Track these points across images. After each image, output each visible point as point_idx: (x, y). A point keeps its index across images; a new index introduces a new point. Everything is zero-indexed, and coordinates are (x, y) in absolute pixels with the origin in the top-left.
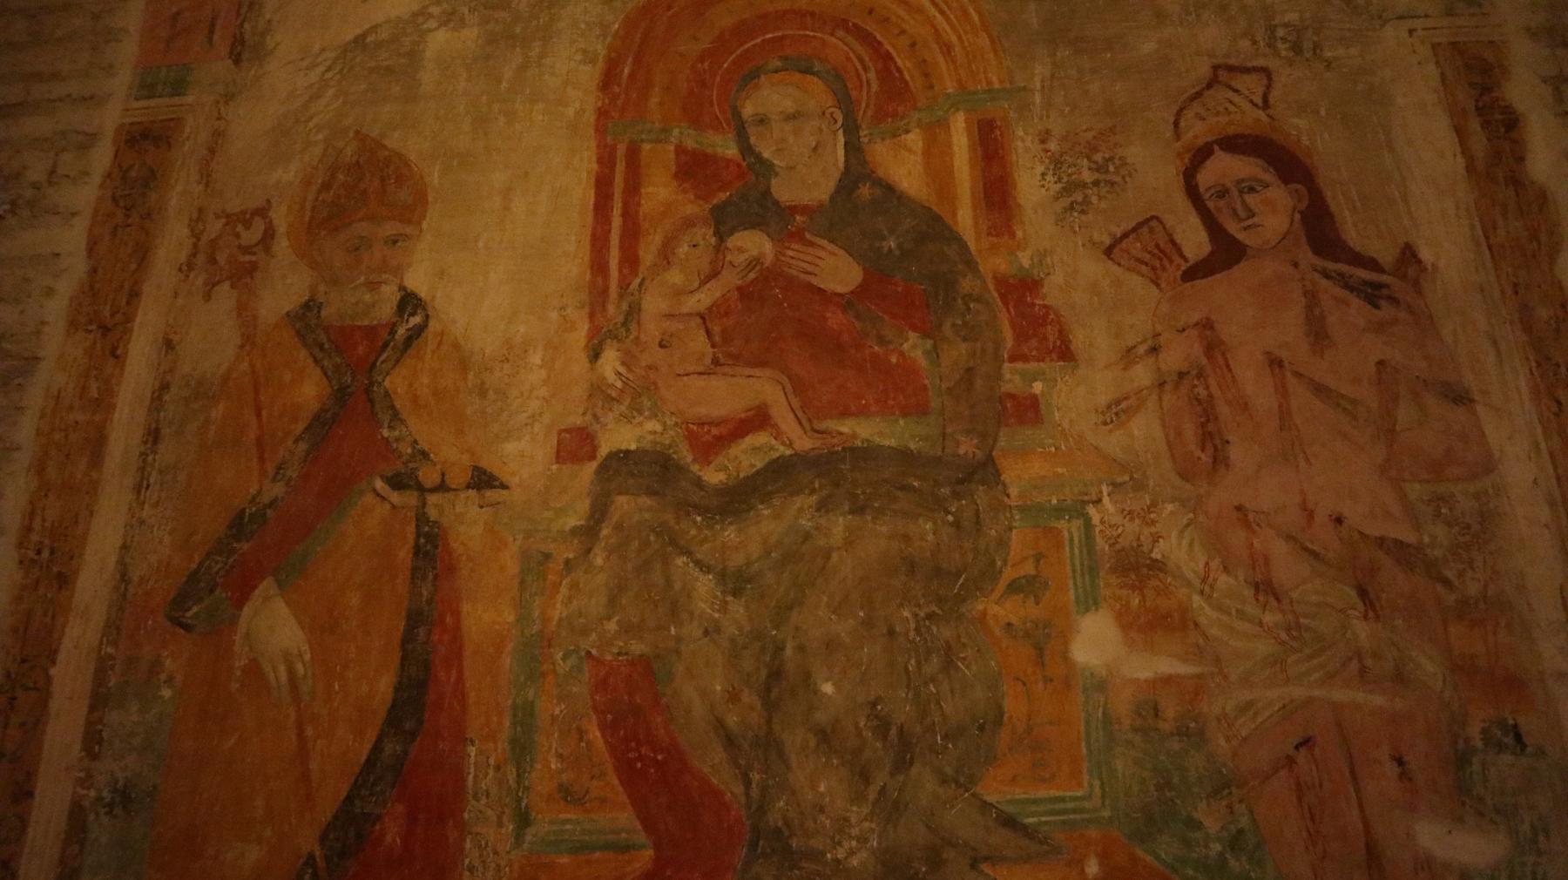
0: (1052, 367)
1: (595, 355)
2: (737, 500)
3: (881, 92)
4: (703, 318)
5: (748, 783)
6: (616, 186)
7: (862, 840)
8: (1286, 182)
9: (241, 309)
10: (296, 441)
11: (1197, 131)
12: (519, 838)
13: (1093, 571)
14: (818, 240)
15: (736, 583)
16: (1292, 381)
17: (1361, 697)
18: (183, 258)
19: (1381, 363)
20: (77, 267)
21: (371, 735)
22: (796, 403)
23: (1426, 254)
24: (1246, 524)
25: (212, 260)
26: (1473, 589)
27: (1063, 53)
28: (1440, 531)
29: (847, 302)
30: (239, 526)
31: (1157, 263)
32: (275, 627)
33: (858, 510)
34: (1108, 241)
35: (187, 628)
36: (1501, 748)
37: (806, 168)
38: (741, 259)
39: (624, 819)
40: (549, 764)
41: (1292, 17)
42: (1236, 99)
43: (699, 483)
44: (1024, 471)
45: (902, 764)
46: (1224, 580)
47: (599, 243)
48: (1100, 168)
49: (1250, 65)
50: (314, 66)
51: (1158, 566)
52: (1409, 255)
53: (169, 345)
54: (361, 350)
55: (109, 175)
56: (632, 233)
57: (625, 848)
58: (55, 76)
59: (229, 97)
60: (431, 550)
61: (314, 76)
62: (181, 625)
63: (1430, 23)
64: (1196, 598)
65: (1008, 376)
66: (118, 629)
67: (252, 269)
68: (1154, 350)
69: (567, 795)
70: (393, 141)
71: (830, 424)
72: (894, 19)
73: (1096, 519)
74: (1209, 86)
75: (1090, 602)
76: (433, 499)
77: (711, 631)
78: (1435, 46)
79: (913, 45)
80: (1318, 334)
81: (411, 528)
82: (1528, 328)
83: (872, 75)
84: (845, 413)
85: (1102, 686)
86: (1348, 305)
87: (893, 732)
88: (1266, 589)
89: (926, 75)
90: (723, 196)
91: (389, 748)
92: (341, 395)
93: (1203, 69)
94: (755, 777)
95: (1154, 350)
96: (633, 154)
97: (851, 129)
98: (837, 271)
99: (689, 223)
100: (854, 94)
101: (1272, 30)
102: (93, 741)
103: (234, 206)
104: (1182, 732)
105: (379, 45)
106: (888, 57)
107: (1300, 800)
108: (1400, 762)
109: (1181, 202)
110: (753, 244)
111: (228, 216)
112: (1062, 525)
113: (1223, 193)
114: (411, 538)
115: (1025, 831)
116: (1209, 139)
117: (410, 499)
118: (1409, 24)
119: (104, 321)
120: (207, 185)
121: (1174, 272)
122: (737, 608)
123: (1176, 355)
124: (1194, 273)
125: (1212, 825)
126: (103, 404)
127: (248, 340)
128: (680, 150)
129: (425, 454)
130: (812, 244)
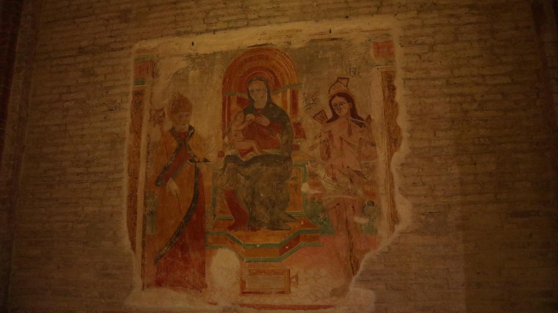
0: (302, 140)
1: (224, 138)
2: (248, 164)
3: (275, 85)
9: (161, 129)
11: (333, 92)
12: (214, 218)
15: (247, 178)
16: (344, 142)
17: (348, 197)
18: (149, 118)
19: (360, 139)
20: (130, 120)
21: (190, 203)
23: (372, 117)
24: (332, 168)
25: (154, 119)
26: (370, 179)
27: (309, 75)
28: (366, 169)
29: (267, 128)
30: (165, 169)
32: (173, 186)
33: (267, 165)
34: (314, 115)
36: (370, 205)
37: (261, 103)
38: (249, 119)
39: (230, 216)
40: (218, 208)
41: (354, 66)
43: (241, 161)
44: (296, 159)
45: (273, 207)
46: (328, 178)
47: (223, 116)
48: (314, 100)
50: (168, 78)
51: (316, 175)
52: (369, 117)
53: (149, 136)
54: (183, 137)
56: (229, 114)
58: (119, 80)
59: (153, 85)
60: (198, 172)
61: (169, 80)
63: (382, 67)
67: (161, 121)
68: (320, 136)
69: (221, 212)
70: (185, 95)
71: (264, 150)
75: (304, 181)
76: (197, 164)
77: (243, 186)
78: (382, 72)
80: (350, 133)
82: (389, 132)
84: (266, 148)
85: (306, 195)
90: (245, 107)
91: (193, 205)
92: (180, 145)
93: (336, 79)
95: (320, 136)
96: (229, 98)
97: (269, 93)
98: (265, 121)
99: (239, 112)
101: (350, 69)
102: (145, 204)
103: (157, 108)
104: (318, 202)
105: (180, 74)
106: (276, 77)
108: (353, 207)
110: (250, 116)
112: (301, 168)
115: (293, 218)
117: (194, 164)
118: (377, 67)
119: (136, 131)
122: (248, 182)
123: (323, 138)
125: (321, 217)
126: (138, 147)
127: (163, 135)
128: (238, 97)
129: (196, 156)
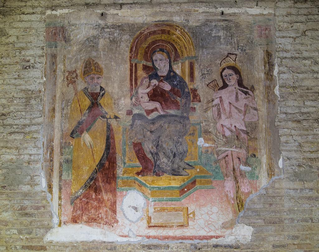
1: (131, 99)
2: (153, 122)
5: (154, 159)
6: (133, 69)
8: (236, 74)
10: (86, 110)
11: (224, 65)
13: (201, 133)
14: (164, 82)
22: (161, 107)
31: (215, 87)
35: (74, 138)
38: (153, 84)
42: (231, 60)
49: (234, 53)
56: (136, 80)
57: (138, 167)
65: (191, 104)
66: (63, 138)
72: (178, 42)
73: (202, 126)
74: (227, 57)
75: (200, 136)
76: (109, 120)
83: (174, 53)
86: (242, 95)
87: (173, 153)
94: (155, 158)
96: (136, 65)
98: (167, 87)
100: (171, 56)
107: (225, 163)
110: (155, 82)
111: (69, 72)
116: (225, 66)
117: (106, 120)
120: (64, 66)
121: (217, 89)
128: (143, 65)
130: (163, 82)
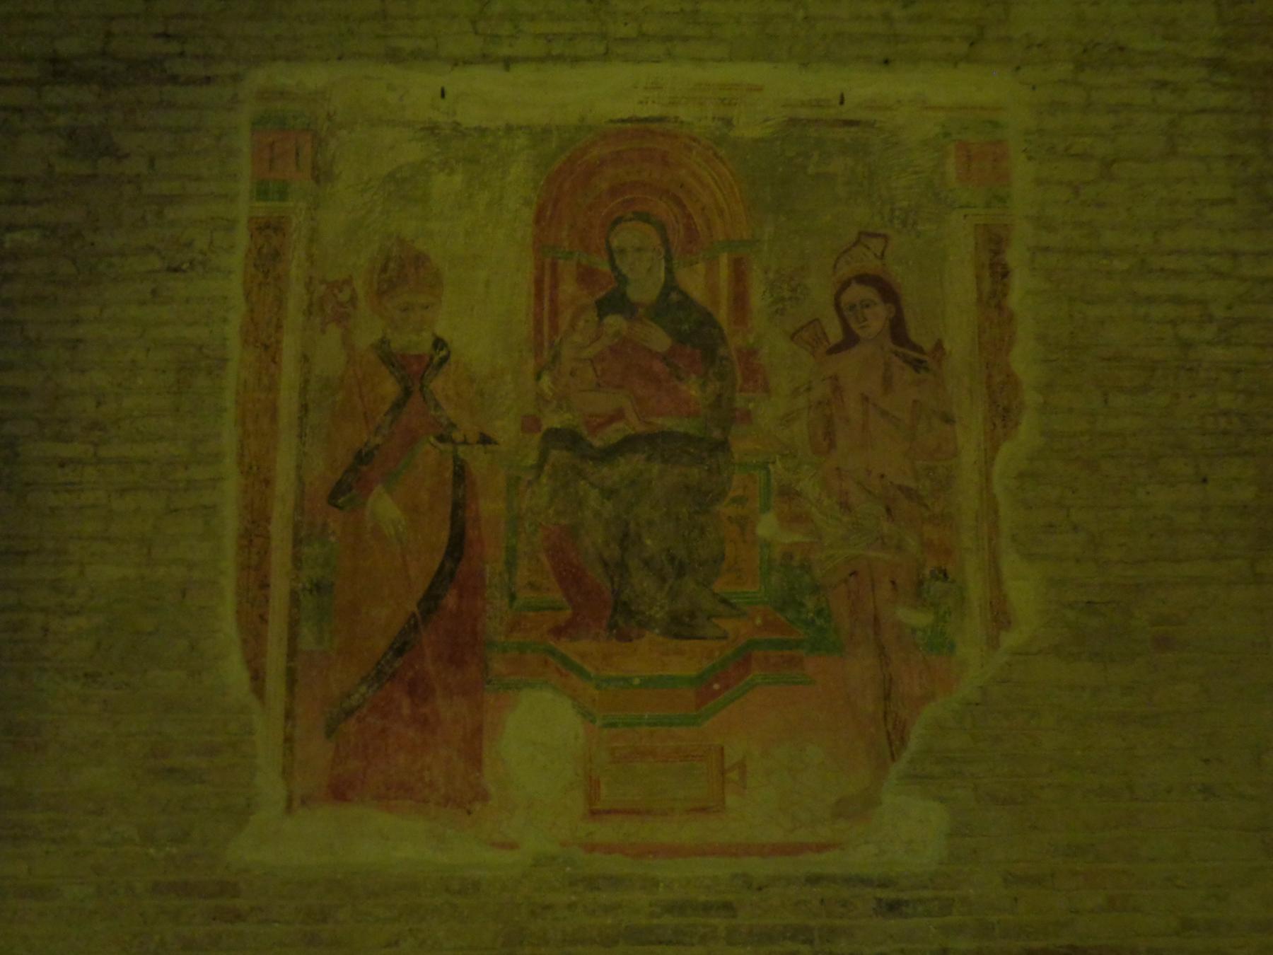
1: (538, 377)
4: (592, 361)
5: (613, 583)
7: (662, 607)
11: (845, 271)
15: (609, 493)
23: (947, 346)
29: (664, 358)
32: (384, 507)
36: (937, 579)
37: (644, 290)
39: (557, 596)
41: (905, 204)
43: (591, 446)
44: (742, 445)
48: (794, 290)
51: (798, 494)
52: (939, 346)
55: (250, 250)
56: (555, 313)
58: (198, 179)
62: (336, 506)
64: (813, 509)
68: (809, 389)
69: (532, 586)
74: (855, 244)
75: (766, 508)
79: (703, 209)
80: (887, 383)
81: (451, 462)
88: (846, 506)
89: (709, 228)
94: (616, 579)
95: (809, 389)
96: (554, 266)
97: (668, 259)
101: (892, 210)
102: (297, 560)
106: (689, 217)
109: (831, 312)
110: (615, 322)
113: (852, 307)
114: (451, 468)
115: (732, 606)
117: (447, 447)
122: (609, 505)
124: (836, 349)
126: (272, 388)
128: (579, 265)
